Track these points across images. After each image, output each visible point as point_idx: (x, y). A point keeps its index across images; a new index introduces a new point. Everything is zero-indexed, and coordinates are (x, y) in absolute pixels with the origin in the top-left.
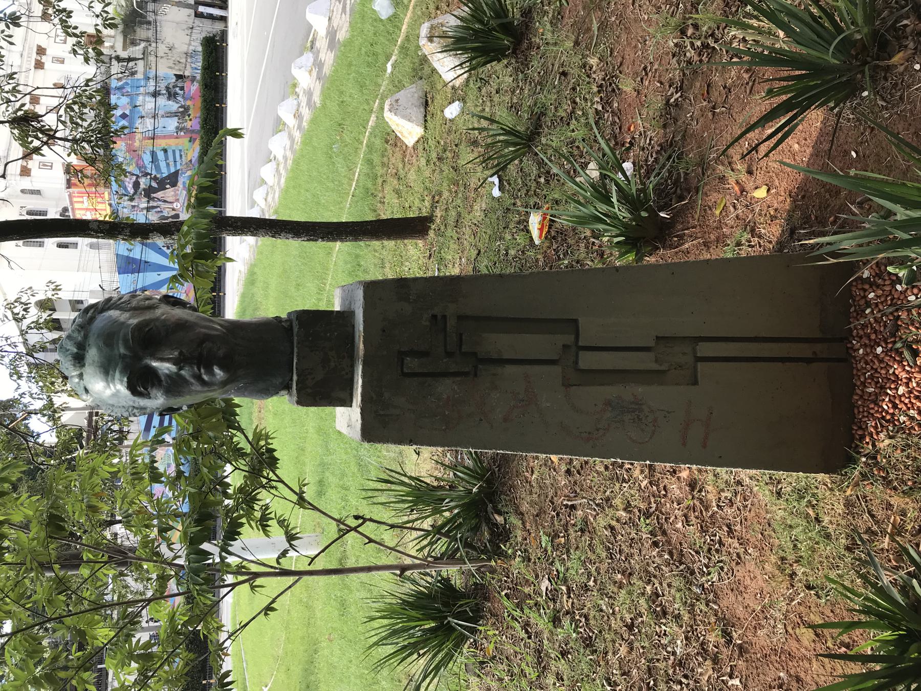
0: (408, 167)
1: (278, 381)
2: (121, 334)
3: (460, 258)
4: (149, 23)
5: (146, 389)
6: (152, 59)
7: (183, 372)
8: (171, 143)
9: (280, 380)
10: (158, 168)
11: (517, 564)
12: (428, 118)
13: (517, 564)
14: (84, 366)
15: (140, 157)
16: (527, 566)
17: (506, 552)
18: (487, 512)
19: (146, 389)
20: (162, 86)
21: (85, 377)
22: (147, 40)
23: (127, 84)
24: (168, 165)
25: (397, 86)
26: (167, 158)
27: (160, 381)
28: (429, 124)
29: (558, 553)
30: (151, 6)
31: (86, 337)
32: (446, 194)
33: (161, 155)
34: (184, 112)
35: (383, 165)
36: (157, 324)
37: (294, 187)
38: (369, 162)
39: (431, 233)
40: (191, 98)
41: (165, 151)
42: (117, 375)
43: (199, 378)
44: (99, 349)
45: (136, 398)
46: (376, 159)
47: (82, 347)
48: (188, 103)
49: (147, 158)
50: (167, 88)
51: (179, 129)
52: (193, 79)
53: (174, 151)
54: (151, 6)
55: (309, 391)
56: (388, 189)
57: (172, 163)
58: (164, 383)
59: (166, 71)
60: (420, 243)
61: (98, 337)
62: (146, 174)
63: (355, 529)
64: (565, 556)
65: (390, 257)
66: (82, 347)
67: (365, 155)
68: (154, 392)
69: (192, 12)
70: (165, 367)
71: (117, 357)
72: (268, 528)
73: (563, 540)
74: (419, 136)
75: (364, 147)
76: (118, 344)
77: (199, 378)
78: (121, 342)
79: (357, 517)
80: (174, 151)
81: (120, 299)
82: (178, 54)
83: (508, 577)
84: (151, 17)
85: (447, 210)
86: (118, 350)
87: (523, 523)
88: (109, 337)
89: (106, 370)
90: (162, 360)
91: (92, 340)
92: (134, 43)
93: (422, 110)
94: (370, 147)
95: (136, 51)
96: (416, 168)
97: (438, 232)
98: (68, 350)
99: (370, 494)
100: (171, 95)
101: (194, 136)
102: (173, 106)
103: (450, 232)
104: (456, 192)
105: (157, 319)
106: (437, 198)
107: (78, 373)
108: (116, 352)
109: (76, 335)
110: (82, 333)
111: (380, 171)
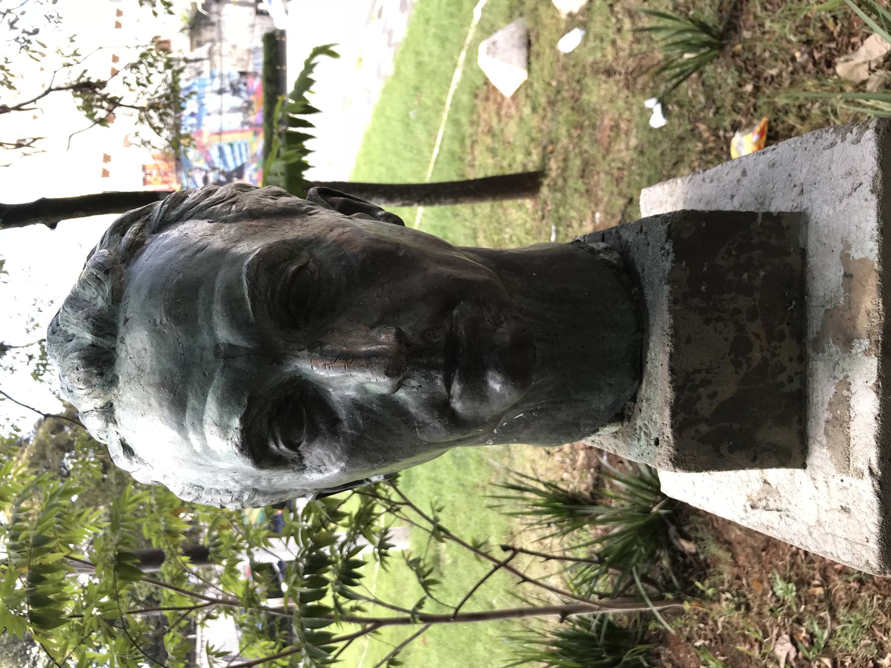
0: (505, 120)
1: (602, 402)
2: (219, 285)
3: (593, 213)
4: (213, 24)
5: (293, 446)
6: (216, 58)
7: (401, 394)
8: (237, 138)
9: (610, 400)
10: (225, 163)
11: (724, 611)
12: (533, 59)
13: (724, 611)
14: (113, 382)
15: (208, 153)
16: (746, 615)
17: (703, 592)
18: (667, 535)
19: (293, 446)
20: (227, 83)
21: (119, 413)
22: (212, 41)
23: (194, 84)
24: (234, 159)
25: (487, 29)
26: (233, 152)
27: (333, 420)
28: (535, 66)
29: (810, 608)
30: (214, 8)
31: (117, 297)
32: (564, 141)
33: (227, 150)
34: (247, 108)
35: (472, 123)
36: (319, 253)
37: (365, 164)
38: (455, 123)
39: (545, 191)
40: (254, 93)
41: (231, 145)
42: (211, 409)
43: (441, 408)
44: (156, 332)
45: (264, 473)
46: (464, 119)
47: (106, 326)
48: (252, 98)
49: (214, 154)
50: (232, 85)
51: (244, 123)
52: (255, 74)
53: (240, 146)
54: (214, 8)
55: (704, 428)
56: (478, 149)
57: (238, 157)
58: (346, 428)
59: (230, 67)
60: (528, 203)
61: (151, 294)
62: (214, 169)
63: (504, 564)
64: (825, 614)
65: (485, 226)
66: (106, 326)
67: (449, 116)
68: (315, 453)
69: (252, 10)
70: (347, 383)
71: (209, 355)
72: (387, 559)
73: (819, 591)
74: (521, 82)
75: (448, 107)
76: (209, 318)
77: (441, 408)
78: (217, 307)
79: (505, 548)
80: (240, 146)
81: (209, 193)
82: (241, 51)
83: (706, 624)
84: (214, 18)
85: (565, 160)
86: (212, 329)
87: (734, 557)
88: (184, 295)
89: (179, 394)
90: (350, 359)
91: (133, 305)
92: (199, 44)
93: (524, 51)
94: (455, 106)
95: (202, 52)
96: (517, 119)
97: (554, 188)
98: (69, 339)
99: (496, 502)
100: (236, 91)
101: (259, 129)
102: (238, 102)
103: (575, 183)
104: (579, 136)
105: (314, 242)
106: (550, 148)
107: (99, 403)
108: (205, 339)
109: (89, 293)
110: (107, 288)
111: (468, 130)
